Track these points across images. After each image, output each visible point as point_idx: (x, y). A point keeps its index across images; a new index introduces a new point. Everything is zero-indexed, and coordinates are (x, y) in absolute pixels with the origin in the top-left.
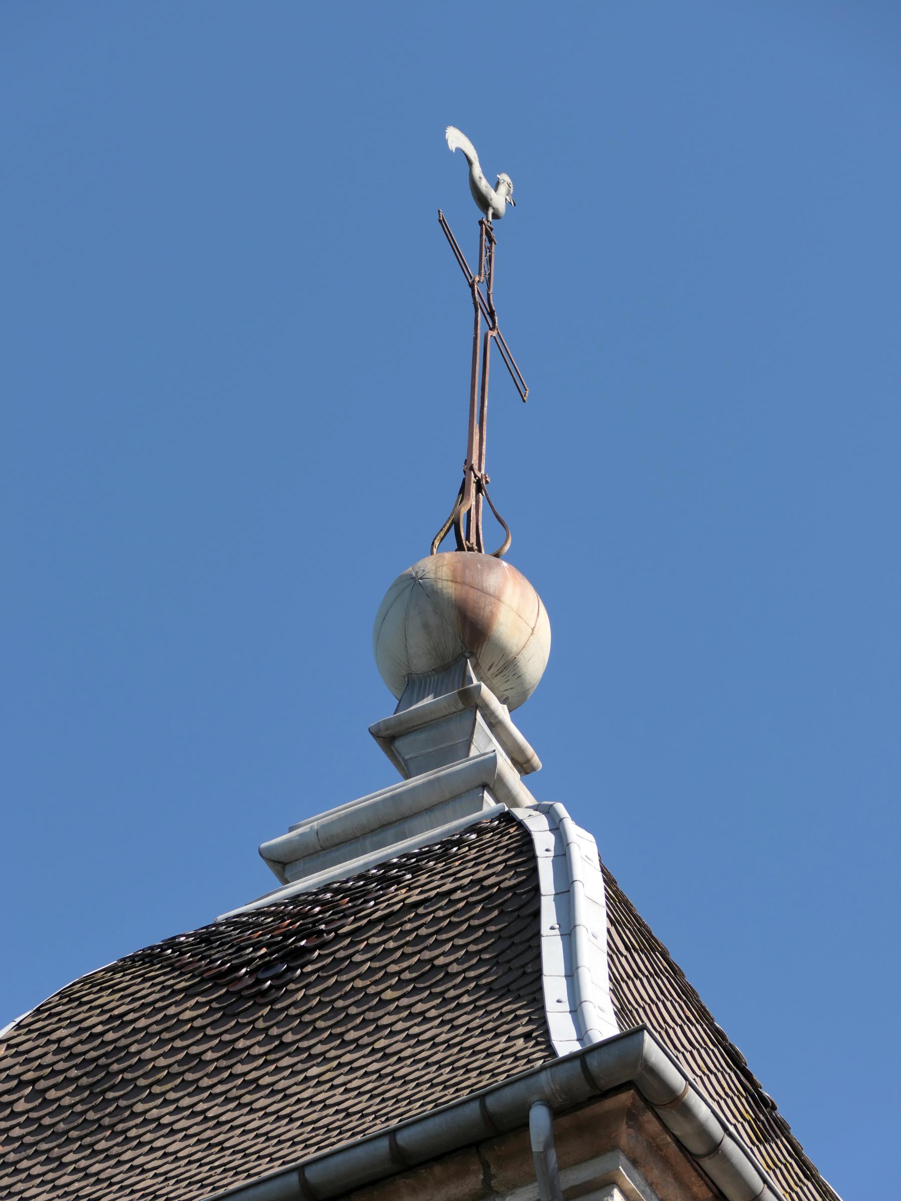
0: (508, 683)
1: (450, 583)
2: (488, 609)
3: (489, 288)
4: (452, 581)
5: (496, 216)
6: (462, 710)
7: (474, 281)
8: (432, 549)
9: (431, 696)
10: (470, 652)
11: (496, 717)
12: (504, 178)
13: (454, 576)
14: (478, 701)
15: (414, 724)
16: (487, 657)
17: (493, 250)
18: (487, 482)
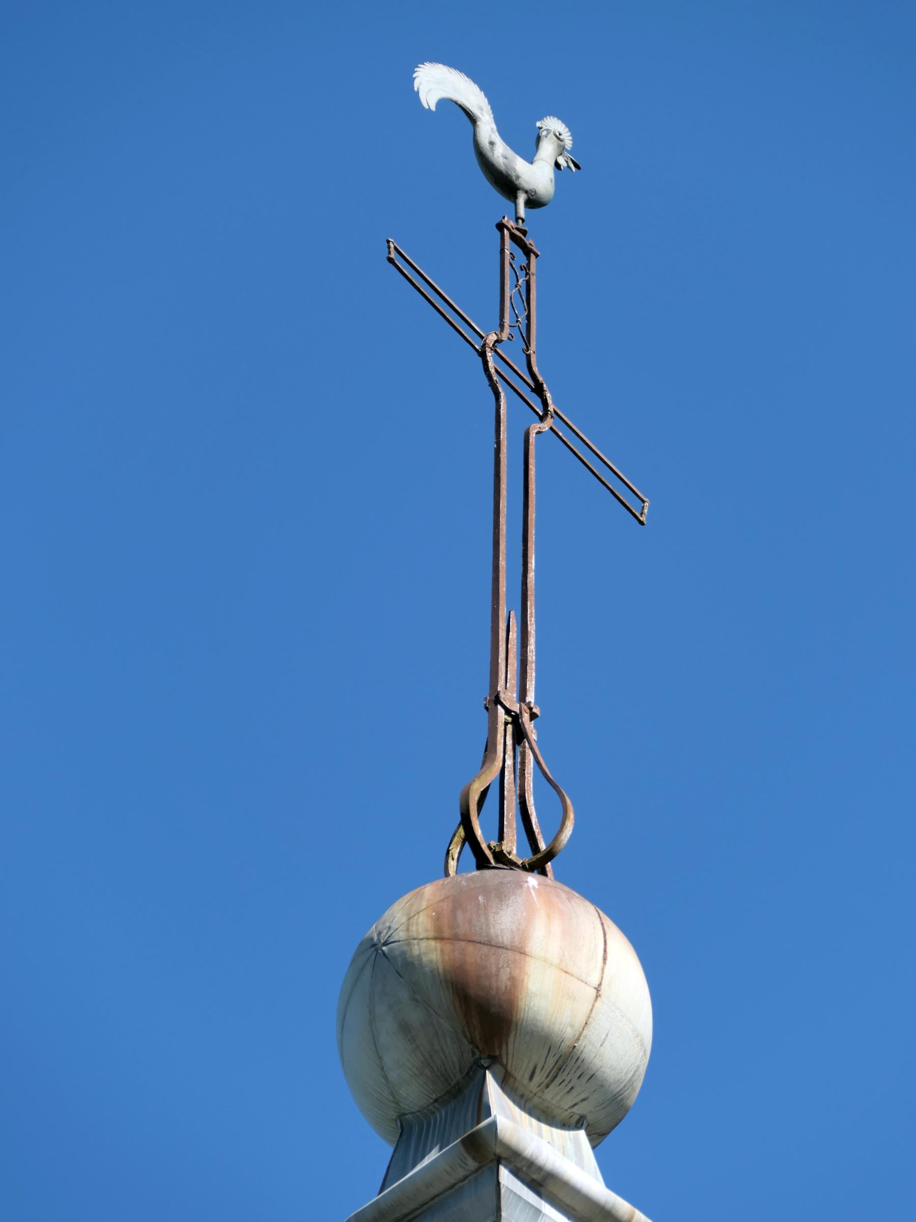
0: (574, 1092)
1: (433, 943)
2: (504, 976)
3: (528, 343)
4: (435, 939)
5: (534, 202)
6: (477, 1170)
7: (484, 346)
8: (447, 862)
9: (437, 1148)
10: (490, 1057)
11: (540, 1169)
12: (553, 124)
13: (438, 929)
14: (498, 1150)
15: (406, 1211)
16: (520, 1058)
17: (533, 269)
18: (533, 716)
